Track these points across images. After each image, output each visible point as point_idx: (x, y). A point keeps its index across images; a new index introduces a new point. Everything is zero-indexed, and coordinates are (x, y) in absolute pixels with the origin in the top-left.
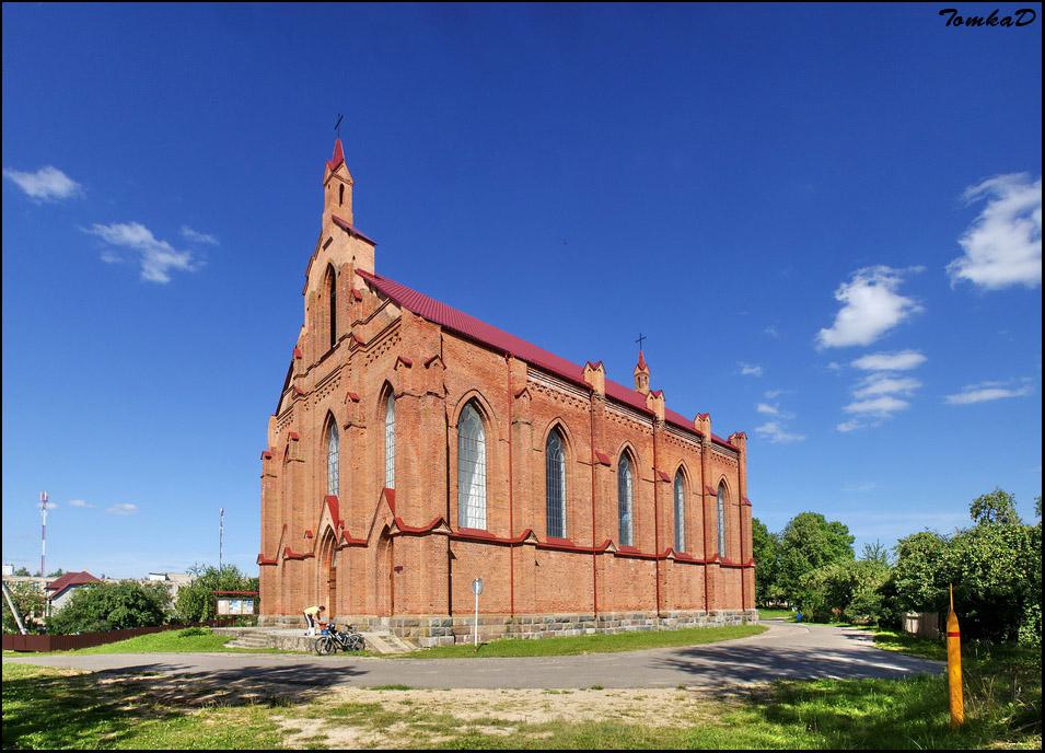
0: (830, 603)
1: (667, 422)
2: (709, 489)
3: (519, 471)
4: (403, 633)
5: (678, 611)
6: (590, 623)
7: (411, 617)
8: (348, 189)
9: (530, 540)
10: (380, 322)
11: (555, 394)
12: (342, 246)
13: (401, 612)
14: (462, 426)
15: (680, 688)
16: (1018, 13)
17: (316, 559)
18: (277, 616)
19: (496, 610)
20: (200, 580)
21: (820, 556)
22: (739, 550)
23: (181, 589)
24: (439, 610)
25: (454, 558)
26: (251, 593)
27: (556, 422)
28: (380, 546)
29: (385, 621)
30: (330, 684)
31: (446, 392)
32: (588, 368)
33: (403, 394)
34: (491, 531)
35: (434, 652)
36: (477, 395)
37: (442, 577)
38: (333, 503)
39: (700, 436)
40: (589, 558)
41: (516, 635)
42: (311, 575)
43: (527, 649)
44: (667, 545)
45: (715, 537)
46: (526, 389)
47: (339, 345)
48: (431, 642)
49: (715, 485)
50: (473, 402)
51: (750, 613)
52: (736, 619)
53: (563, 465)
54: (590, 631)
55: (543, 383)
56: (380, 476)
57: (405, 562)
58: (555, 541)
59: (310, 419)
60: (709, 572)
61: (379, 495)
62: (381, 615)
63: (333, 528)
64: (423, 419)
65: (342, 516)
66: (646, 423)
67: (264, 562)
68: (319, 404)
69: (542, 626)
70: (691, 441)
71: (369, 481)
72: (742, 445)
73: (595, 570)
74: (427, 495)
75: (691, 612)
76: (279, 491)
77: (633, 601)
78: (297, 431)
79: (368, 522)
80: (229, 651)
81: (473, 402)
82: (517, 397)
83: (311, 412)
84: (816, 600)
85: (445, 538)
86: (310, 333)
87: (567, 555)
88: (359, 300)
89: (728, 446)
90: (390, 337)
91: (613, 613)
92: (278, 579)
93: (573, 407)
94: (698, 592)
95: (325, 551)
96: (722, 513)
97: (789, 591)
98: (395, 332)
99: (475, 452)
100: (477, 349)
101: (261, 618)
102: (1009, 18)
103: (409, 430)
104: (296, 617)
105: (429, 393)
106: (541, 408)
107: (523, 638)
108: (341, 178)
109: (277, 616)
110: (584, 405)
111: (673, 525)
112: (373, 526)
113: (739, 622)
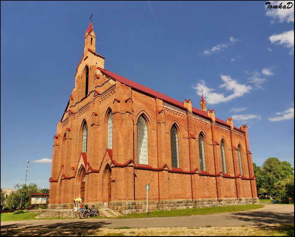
0: (288, 195)
1: (216, 122)
2: (234, 147)
3: (161, 141)
4: (115, 209)
5: (226, 198)
6: (191, 203)
7: (119, 201)
8: (94, 39)
9: (166, 169)
10: (107, 86)
11: (174, 112)
12: (92, 59)
13: (114, 199)
14: (139, 124)
15: (243, 226)
16: (288, 4)
17: (76, 179)
18: (57, 204)
19: (153, 198)
20: (20, 190)
21: (280, 176)
22: (248, 172)
23: (225, 87)
24: (130, 198)
25: (136, 176)
26: (45, 194)
27: (174, 122)
28: (105, 172)
29: (106, 204)
30: (98, 228)
31: (133, 111)
32: (185, 102)
33: (117, 112)
34: (150, 165)
35: (129, 216)
36: (144, 113)
37: (131, 184)
38: (84, 156)
39: (229, 127)
40: (189, 176)
41: (161, 209)
42: (73, 186)
43: (168, 214)
44: (220, 171)
45: (238, 167)
46: (163, 110)
47: (89, 95)
48: (127, 212)
49: (237, 146)
50: (143, 115)
51: (255, 199)
52: (250, 202)
53: (177, 139)
54: (191, 207)
55: (169, 108)
56: (105, 144)
57: (116, 178)
58: (175, 169)
59: (77, 122)
60: (237, 181)
61: (105, 152)
62: (104, 201)
63: (84, 165)
64: (124, 122)
65: (88, 160)
66: (208, 122)
67: (52, 181)
68: (80, 117)
69: (171, 204)
70: (226, 129)
71: (100, 146)
72: (246, 130)
73: (191, 181)
74: (126, 151)
75: (231, 199)
76: (60, 151)
77: (207, 194)
78: (70, 127)
79: (100, 162)
80: (37, 219)
81: (143, 115)
82: (159, 113)
83: (76, 120)
84: (281, 194)
85: (133, 168)
86: (78, 90)
87: (180, 175)
88: (98, 78)
89: (240, 130)
90: (111, 91)
91: (200, 199)
92: (58, 188)
93: (180, 116)
94: (233, 190)
95: (80, 175)
96: (240, 157)
97: (269, 190)
98: (113, 90)
99: (143, 134)
100: (144, 95)
101: (50, 205)
102: (285, 6)
103: (119, 126)
104: (66, 204)
105: (127, 112)
106: (168, 117)
107: (164, 210)
108: (92, 36)
109: (57, 204)
110: (184, 116)
111: (221, 162)
112: (102, 164)
113: (251, 203)
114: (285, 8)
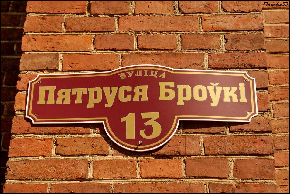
16: (283, 3)
102: (282, 4)
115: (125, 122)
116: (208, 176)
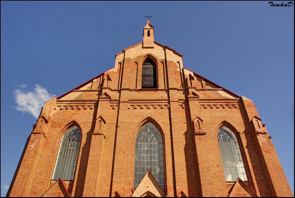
16: (288, 3)
77: (50, 140)
102: (286, 4)
114: (286, 6)
115: (116, 193)
116: (110, 182)
